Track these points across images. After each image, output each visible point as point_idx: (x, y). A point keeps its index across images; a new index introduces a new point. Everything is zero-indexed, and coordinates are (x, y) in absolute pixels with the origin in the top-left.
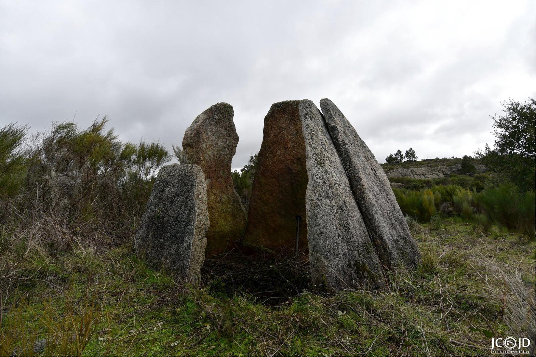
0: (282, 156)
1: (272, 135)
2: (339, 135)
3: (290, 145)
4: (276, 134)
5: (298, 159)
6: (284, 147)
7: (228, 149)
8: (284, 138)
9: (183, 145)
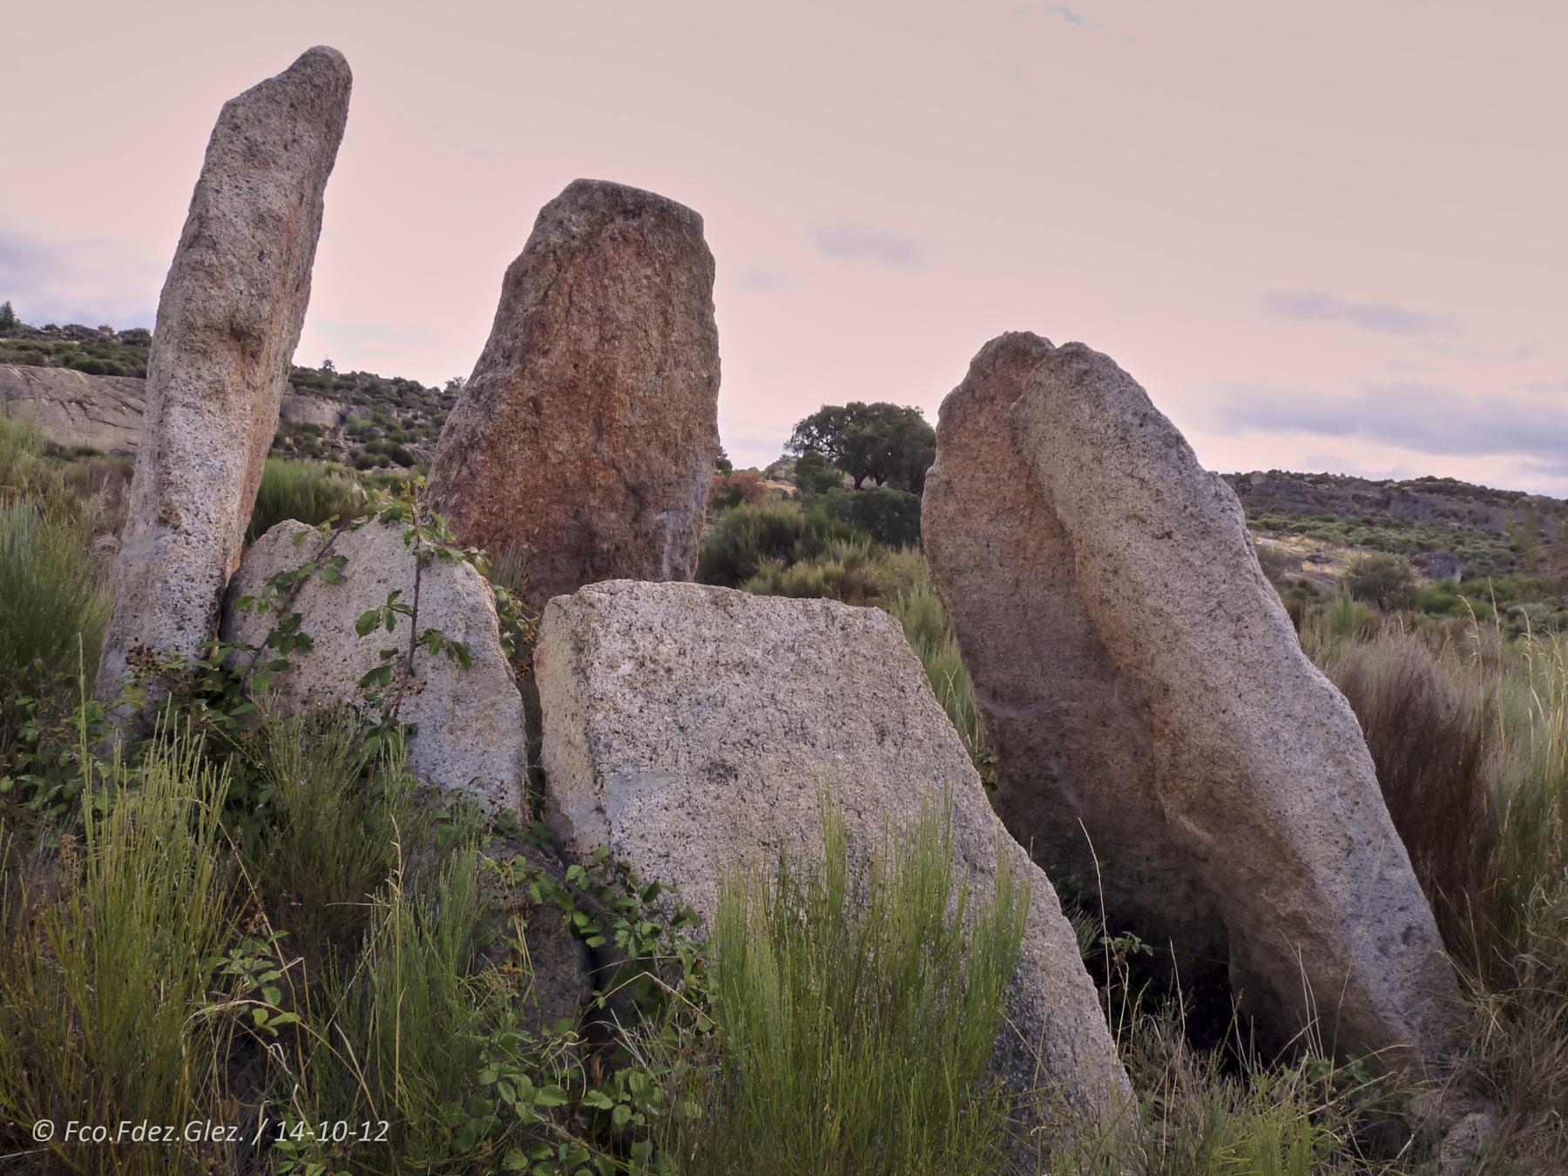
1: (562, 345)
3: (625, 416)
8: (610, 379)
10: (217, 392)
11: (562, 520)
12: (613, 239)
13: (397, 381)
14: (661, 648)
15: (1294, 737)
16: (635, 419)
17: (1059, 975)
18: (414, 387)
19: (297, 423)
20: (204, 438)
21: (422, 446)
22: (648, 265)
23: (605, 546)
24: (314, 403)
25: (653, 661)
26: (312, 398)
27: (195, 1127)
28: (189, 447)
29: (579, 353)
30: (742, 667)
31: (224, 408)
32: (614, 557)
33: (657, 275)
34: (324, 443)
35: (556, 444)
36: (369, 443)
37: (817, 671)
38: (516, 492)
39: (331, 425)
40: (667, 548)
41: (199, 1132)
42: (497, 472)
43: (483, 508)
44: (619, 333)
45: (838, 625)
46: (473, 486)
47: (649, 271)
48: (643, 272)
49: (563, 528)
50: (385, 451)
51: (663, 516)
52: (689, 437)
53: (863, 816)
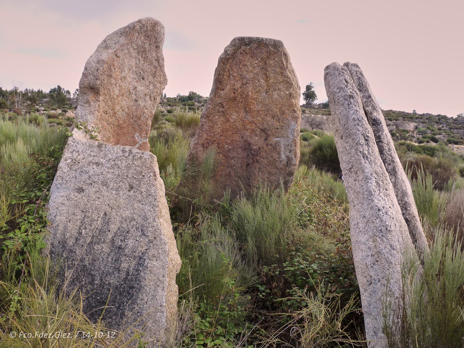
1: (228, 87)
3: (256, 107)
4: (236, 87)
5: (263, 130)
6: (245, 109)
7: (150, 97)
8: (247, 96)
10: (88, 102)
11: (238, 139)
12: (241, 53)
13: (439, 115)
14: (79, 157)
15: (364, 226)
16: (258, 108)
17: (155, 275)
18: (445, 117)
19: (401, 129)
20: (83, 112)
21: (443, 136)
22: (256, 60)
23: (255, 147)
24: (408, 123)
25: (75, 160)
26: (407, 122)
28: (79, 115)
29: (234, 89)
30: (97, 164)
31: (90, 106)
32: (259, 151)
33: (260, 62)
34: (409, 136)
35: (232, 116)
36: (424, 135)
37: (119, 167)
38: (219, 130)
39: (412, 130)
40: (282, 149)
44: (248, 82)
45: (132, 155)
47: (257, 62)
48: (255, 62)
49: (238, 141)
50: (429, 138)
51: (278, 139)
52: (283, 113)
53: (113, 210)
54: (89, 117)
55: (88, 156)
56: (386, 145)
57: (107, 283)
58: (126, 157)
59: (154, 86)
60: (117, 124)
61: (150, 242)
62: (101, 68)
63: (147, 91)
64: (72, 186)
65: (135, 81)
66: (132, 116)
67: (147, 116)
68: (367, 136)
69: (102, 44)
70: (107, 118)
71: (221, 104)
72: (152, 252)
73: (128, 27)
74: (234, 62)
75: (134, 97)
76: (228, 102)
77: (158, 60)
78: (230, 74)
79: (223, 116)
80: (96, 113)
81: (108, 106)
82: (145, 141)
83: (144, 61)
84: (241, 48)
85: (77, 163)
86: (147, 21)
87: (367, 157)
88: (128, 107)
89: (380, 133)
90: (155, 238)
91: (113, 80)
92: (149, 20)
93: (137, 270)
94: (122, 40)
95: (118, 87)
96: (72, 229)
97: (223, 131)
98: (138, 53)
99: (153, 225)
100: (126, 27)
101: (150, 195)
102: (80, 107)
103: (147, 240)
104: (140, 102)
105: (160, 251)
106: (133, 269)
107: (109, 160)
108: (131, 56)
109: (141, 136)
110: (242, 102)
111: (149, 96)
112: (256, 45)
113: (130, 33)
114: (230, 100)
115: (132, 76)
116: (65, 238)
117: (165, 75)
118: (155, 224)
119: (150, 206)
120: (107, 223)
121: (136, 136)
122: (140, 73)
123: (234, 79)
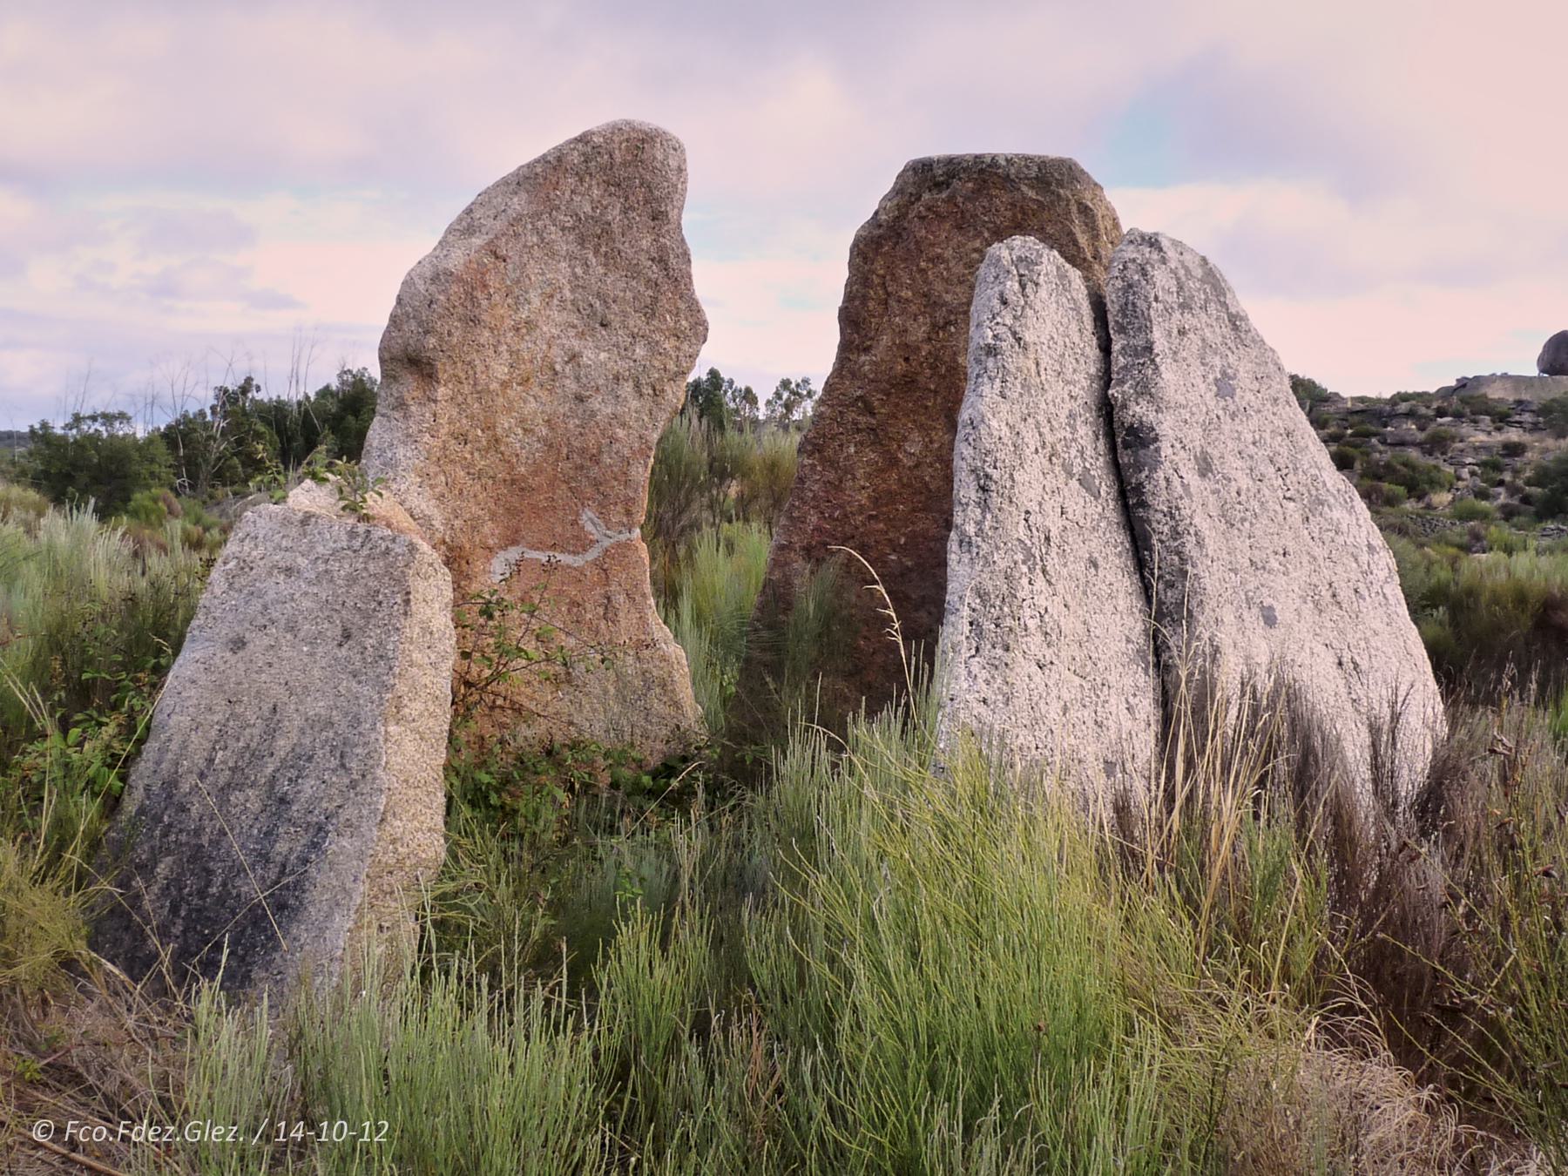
0: (931, 465)
1: (885, 340)
2: (1161, 474)
4: (911, 339)
7: (637, 386)
9: (382, 361)
10: (401, 405)
12: (922, 218)
27: (197, 1127)
28: (375, 445)
30: (288, 571)
38: (862, 497)
41: (199, 1132)
42: (831, 476)
43: (822, 513)
45: (370, 545)
46: (803, 490)
48: (970, 245)
54: (401, 451)
55: (275, 549)
56: (1159, 516)
57: (234, 892)
58: (355, 551)
59: (653, 346)
60: (508, 477)
61: (353, 785)
62: (442, 298)
63: (622, 366)
64: (224, 632)
65: (572, 333)
66: (565, 451)
67: (626, 452)
68: (987, 476)
69: (460, 219)
70: (468, 456)
71: (865, 402)
72: (349, 813)
73: (543, 159)
74: (900, 252)
75: (571, 385)
76: (888, 395)
77: (661, 261)
78: (888, 294)
79: (873, 443)
80: (425, 440)
81: (471, 417)
82: (623, 538)
83: (606, 265)
84: (919, 199)
85: (247, 570)
86: (613, 133)
87: (970, 543)
88: (548, 421)
89: (1143, 475)
90: (364, 776)
91: (487, 333)
92: (620, 129)
93: (306, 861)
94: (518, 204)
95: (506, 355)
96: (198, 744)
97: (876, 501)
98: (582, 241)
99: (367, 740)
100: (537, 161)
101: (381, 657)
102: (379, 421)
103: (347, 781)
104: (595, 403)
105: (365, 812)
106: (298, 858)
107: (317, 559)
108: (553, 254)
109: (607, 523)
110: (936, 392)
111: (631, 383)
112: (970, 185)
113: (545, 179)
114: (893, 386)
115: (556, 316)
116: (177, 772)
117: (694, 309)
118: (373, 736)
119: (373, 687)
120: (271, 732)
121: (584, 517)
122: (591, 306)
123: (903, 312)
